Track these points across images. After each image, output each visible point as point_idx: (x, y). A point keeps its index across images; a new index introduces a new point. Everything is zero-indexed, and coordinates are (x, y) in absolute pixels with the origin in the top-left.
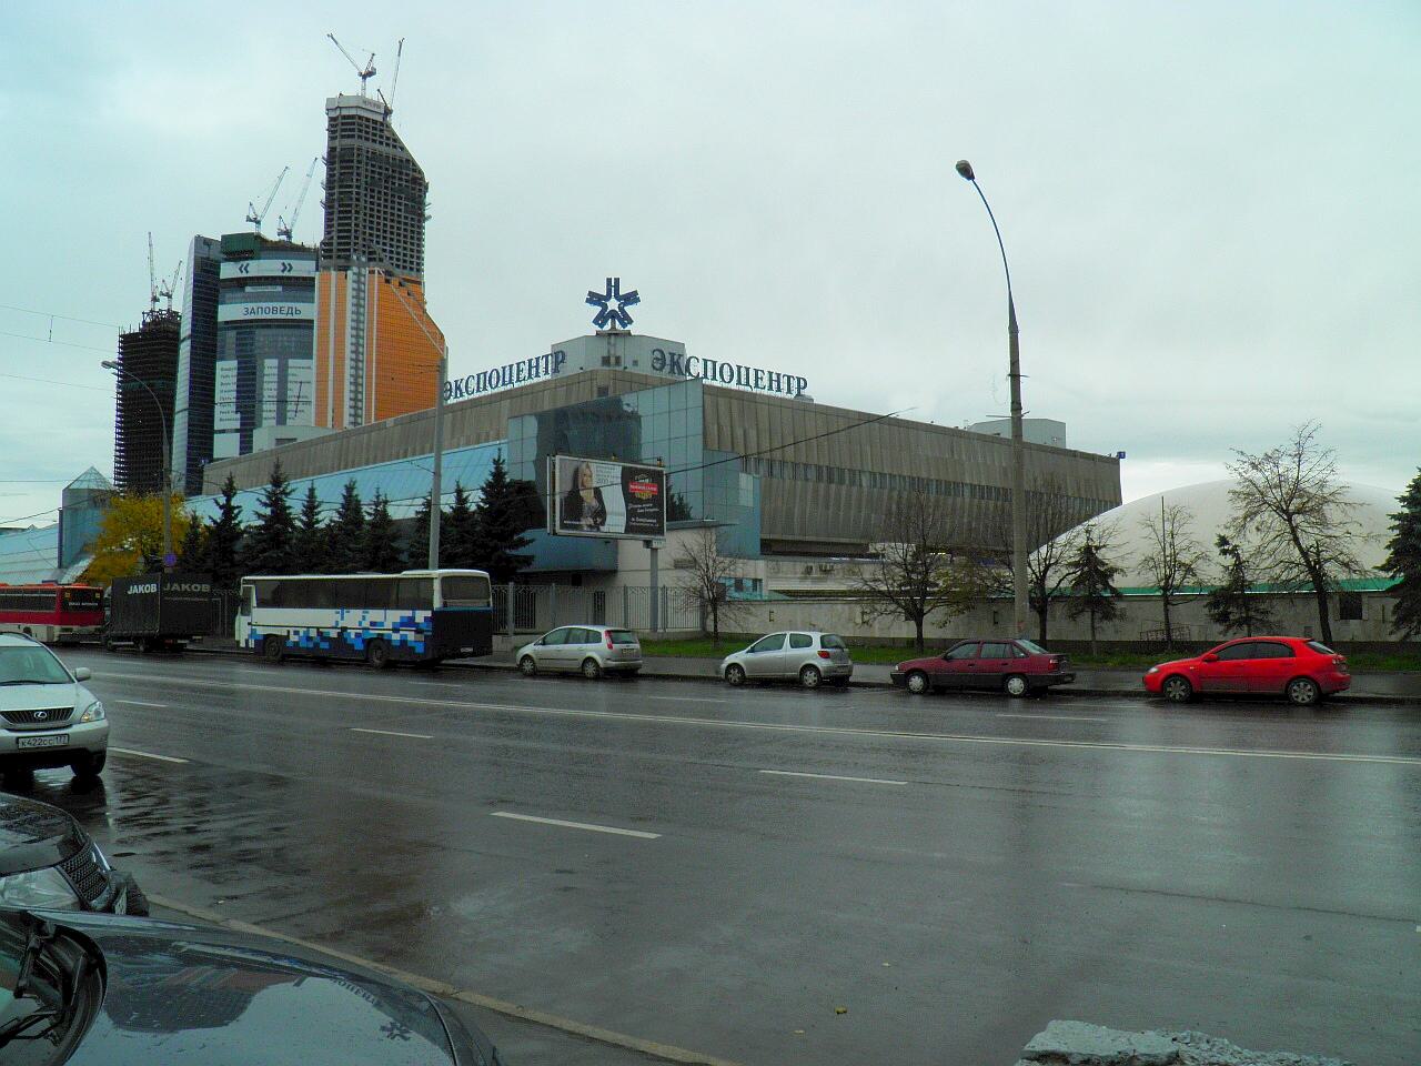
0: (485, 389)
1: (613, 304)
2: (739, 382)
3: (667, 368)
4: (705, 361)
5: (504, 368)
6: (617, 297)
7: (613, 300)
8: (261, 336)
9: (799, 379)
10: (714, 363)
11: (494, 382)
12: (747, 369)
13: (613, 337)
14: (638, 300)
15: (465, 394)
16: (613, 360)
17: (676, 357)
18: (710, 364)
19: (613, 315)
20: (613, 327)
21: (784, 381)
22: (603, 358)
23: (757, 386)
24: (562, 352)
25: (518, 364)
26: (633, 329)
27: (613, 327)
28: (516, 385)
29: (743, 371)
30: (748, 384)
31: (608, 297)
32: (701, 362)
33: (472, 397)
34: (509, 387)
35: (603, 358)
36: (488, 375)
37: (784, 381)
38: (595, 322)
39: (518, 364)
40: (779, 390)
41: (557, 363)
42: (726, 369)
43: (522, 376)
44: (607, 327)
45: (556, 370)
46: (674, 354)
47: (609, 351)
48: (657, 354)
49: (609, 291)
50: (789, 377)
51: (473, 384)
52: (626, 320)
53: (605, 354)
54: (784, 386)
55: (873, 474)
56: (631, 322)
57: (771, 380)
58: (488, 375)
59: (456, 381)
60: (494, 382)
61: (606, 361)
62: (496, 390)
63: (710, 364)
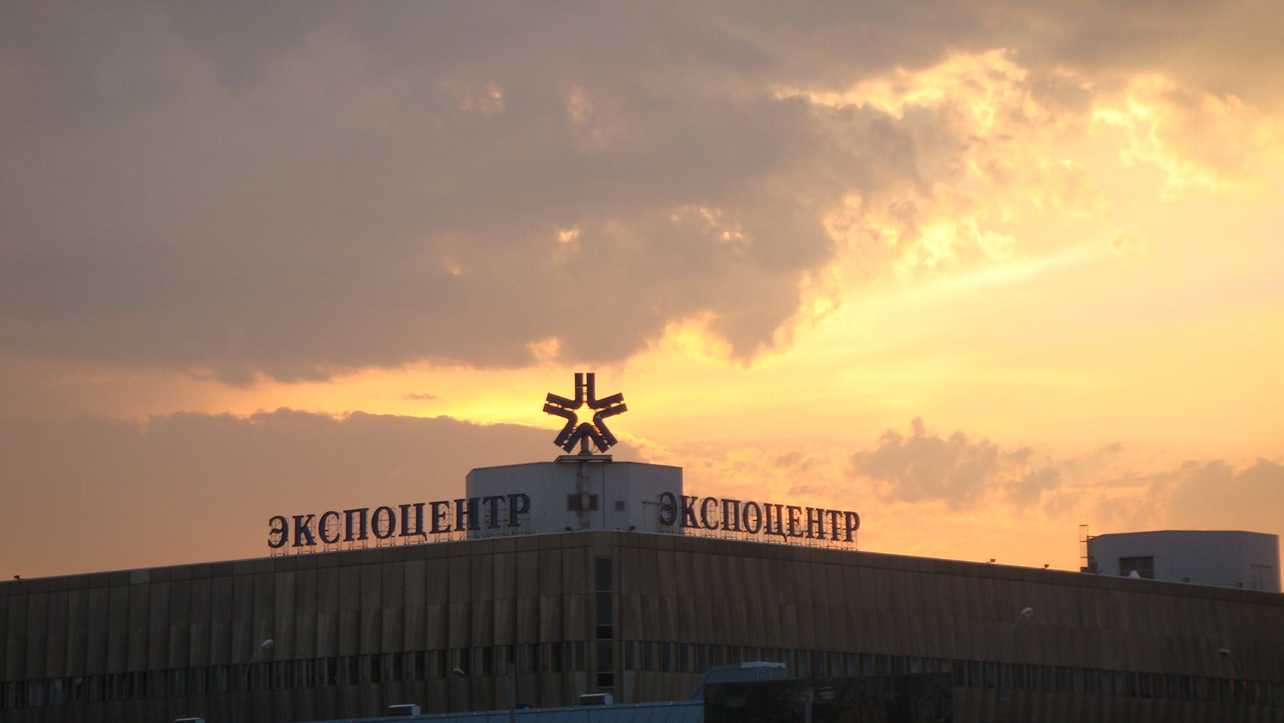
0: (363, 536)
1: (585, 415)
2: (405, 532)
3: (762, 530)
4: (725, 502)
5: (404, 509)
6: (593, 404)
7: (592, 412)
8: (414, 531)
9: (848, 514)
10: (363, 512)
11: (384, 526)
12: (419, 507)
13: (585, 467)
14: (551, 398)
15: (318, 539)
16: (586, 501)
17: (303, 521)
18: (731, 506)
19: (586, 430)
20: (585, 450)
21: (827, 519)
22: (570, 497)
23: (435, 529)
24: (523, 496)
25: (435, 506)
26: (615, 453)
27: (585, 450)
28: (431, 539)
29: (412, 513)
30: (419, 531)
31: (577, 403)
32: (721, 504)
33: (333, 548)
34: (414, 540)
35: (570, 497)
36: (370, 515)
37: (827, 519)
38: (558, 442)
39: (435, 506)
40: (821, 535)
41: (514, 512)
42: (384, 516)
43: (442, 523)
44: (576, 450)
45: (513, 522)
46: (812, 509)
47: (578, 487)
48: (666, 500)
49: (579, 393)
50: (834, 513)
51: (335, 527)
52: (606, 439)
53: (574, 492)
54: (828, 528)
55: (729, 647)
56: (612, 441)
57: (810, 521)
58: (370, 515)
59: (298, 519)
60: (384, 526)
61: (575, 503)
62: (386, 543)
63: (731, 506)
